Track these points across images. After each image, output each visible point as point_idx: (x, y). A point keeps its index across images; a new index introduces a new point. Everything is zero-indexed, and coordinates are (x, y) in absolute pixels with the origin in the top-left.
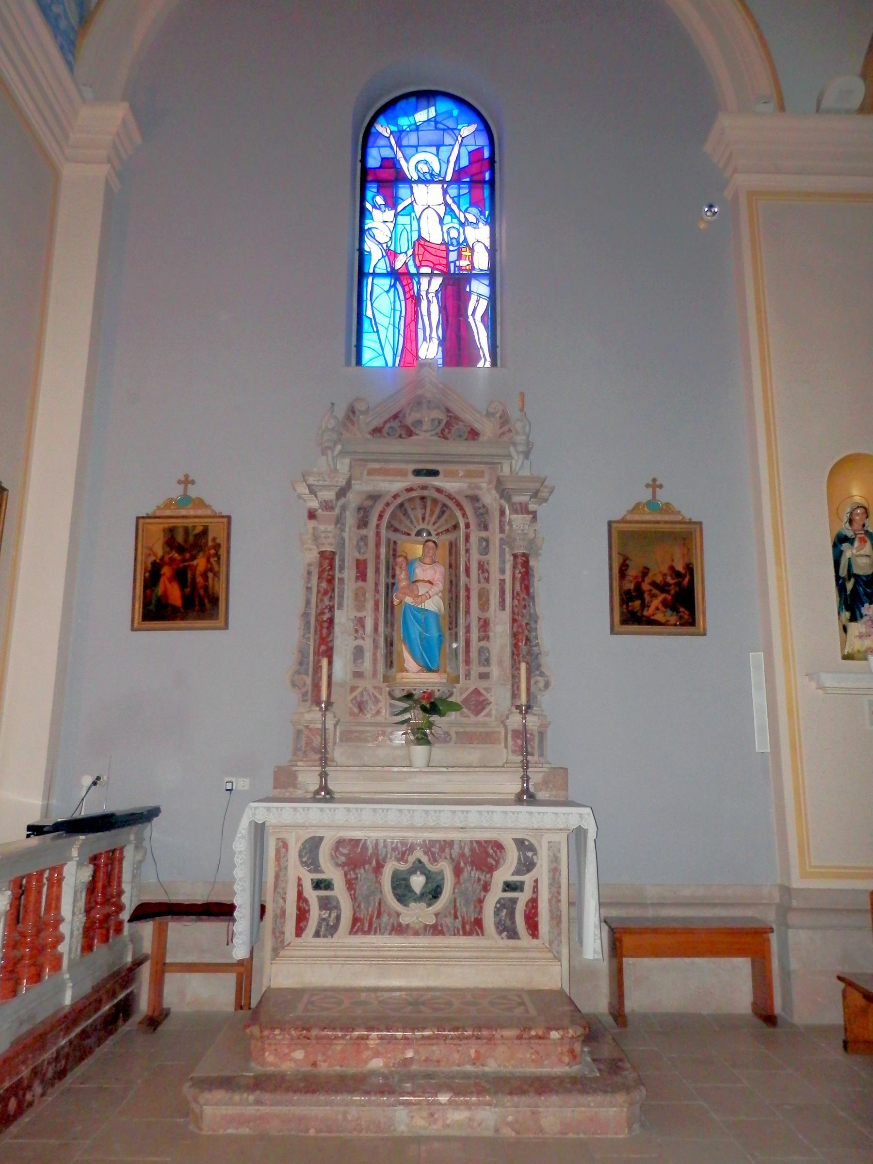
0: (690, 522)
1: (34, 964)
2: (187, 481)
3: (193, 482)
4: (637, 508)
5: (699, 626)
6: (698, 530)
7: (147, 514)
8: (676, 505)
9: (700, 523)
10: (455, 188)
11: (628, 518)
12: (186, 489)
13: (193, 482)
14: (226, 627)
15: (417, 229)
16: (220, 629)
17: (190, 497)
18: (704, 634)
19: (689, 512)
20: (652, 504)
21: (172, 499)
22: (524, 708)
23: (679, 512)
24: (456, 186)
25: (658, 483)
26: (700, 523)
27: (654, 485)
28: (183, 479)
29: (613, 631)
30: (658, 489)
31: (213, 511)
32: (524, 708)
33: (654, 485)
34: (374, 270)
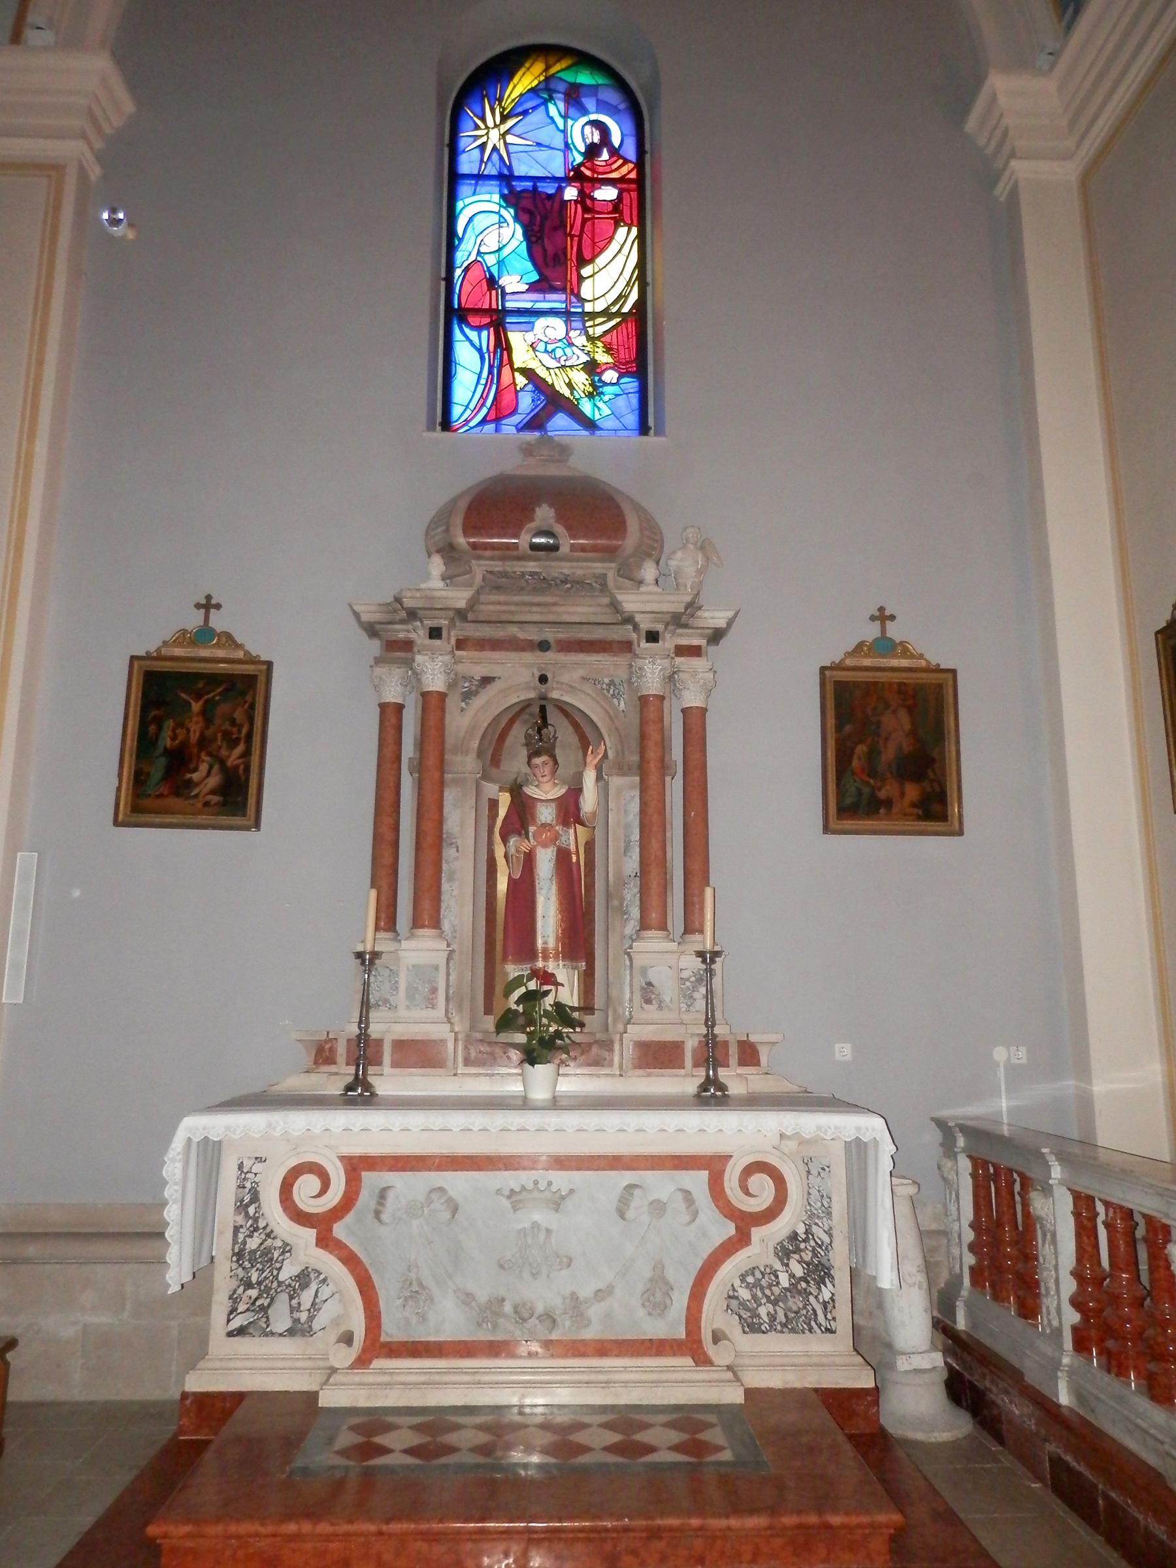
0: (938, 670)
1: (785, 1298)
2: (208, 605)
3: (218, 606)
4: (859, 649)
5: (952, 823)
6: (950, 682)
7: (833, 662)
8: (918, 645)
9: (954, 672)
10: (496, 185)
11: (849, 662)
12: (883, 631)
13: (218, 606)
14: (257, 825)
15: (620, 255)
16: (248, 828)
17: (212, 630)
18: (960, 833)
19: (258, 648)
20: (205, 634)
21: (184, 631)
22: (368, 957)
23: (921, 656)
24: (498, 183)
25: (887, 613)
26: (954, 672)
27: (882, 617)
28: (203, 601)
29: (826, 829)
30: (888, 622)
31: (247, 653)
32: (368, 957)
33: (882, 617)
34: (503, 305)
